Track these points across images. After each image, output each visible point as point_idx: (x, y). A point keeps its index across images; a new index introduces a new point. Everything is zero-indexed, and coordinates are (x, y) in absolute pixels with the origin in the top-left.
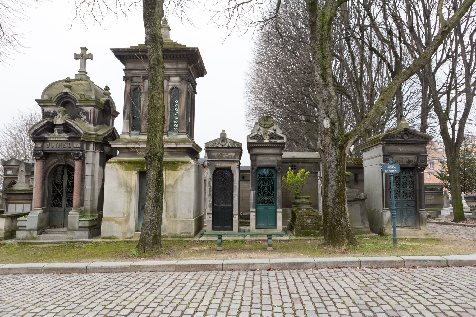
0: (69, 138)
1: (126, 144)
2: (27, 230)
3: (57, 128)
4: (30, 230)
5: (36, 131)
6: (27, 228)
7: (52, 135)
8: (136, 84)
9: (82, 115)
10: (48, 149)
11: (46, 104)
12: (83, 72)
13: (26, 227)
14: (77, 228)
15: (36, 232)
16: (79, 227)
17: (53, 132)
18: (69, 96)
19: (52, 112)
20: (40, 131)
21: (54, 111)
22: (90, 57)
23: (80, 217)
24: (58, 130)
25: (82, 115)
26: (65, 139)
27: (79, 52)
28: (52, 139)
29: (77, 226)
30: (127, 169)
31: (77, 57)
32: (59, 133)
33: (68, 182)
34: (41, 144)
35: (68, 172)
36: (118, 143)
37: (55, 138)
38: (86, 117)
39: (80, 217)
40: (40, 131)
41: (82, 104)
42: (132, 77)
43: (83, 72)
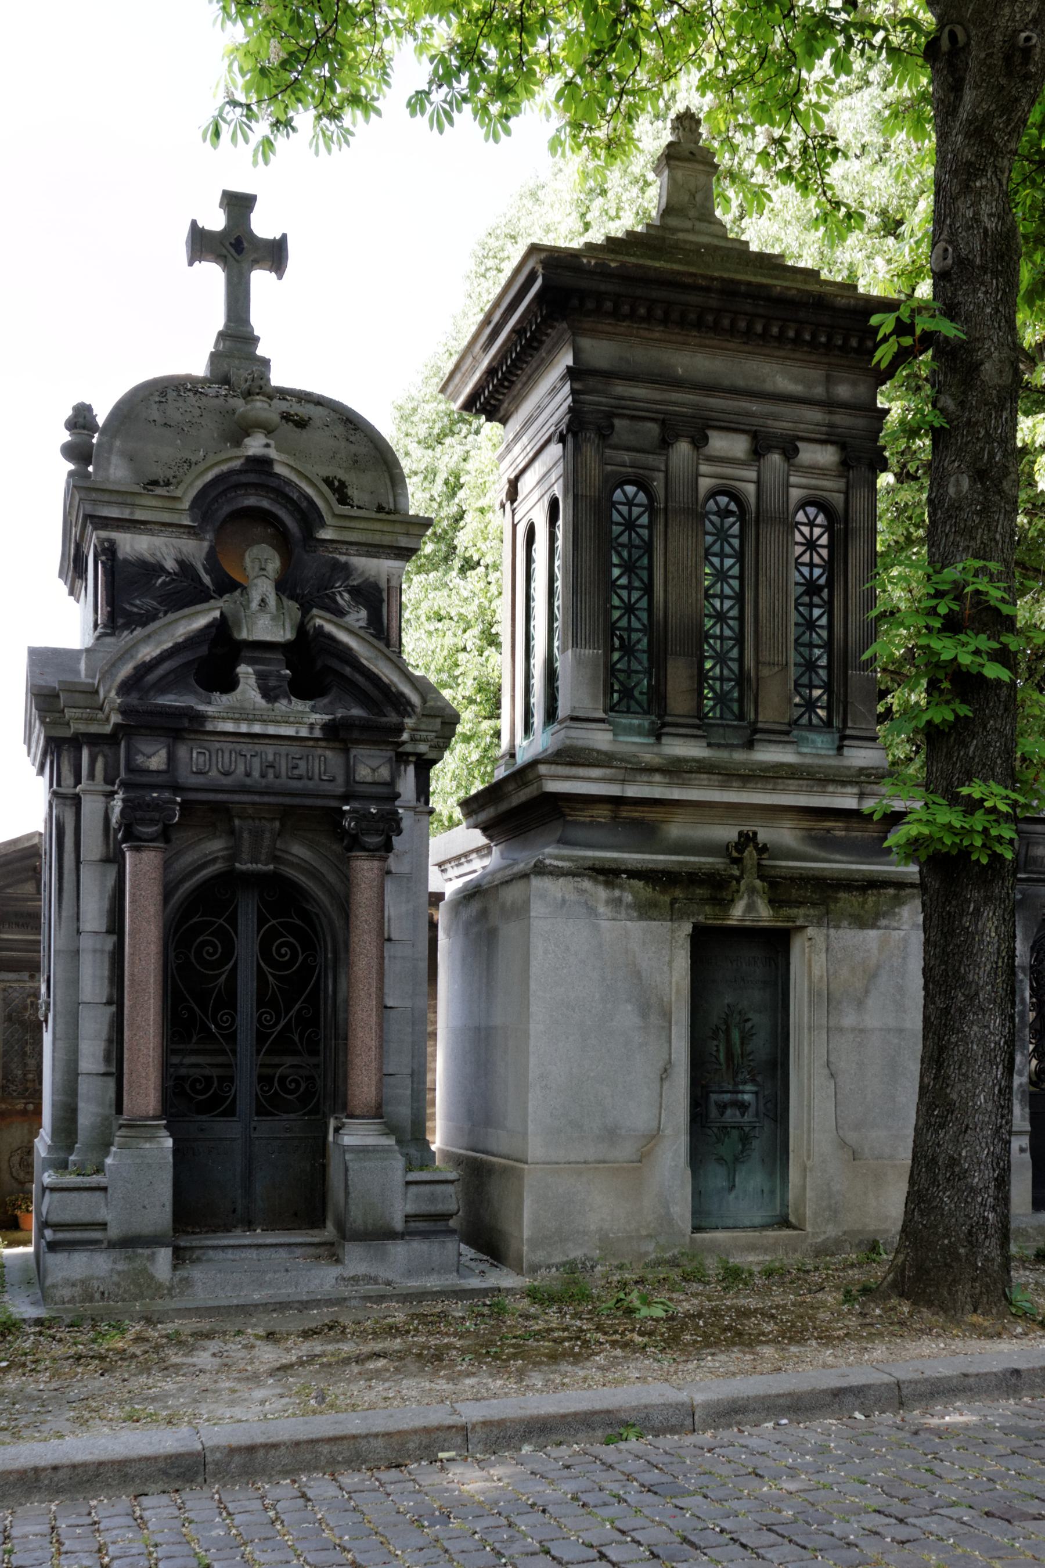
0: (325, 727)
1: (623, 781)
2: (112, 1245)
3: (251, 662)
4: (129, 1243)
5: (145, 669)
6: (114, 1232)
7: (223, 701)
8: (626, 457)
9: (344, 599)
10: (200, 780)
11: (139, 515)
12: (237, 338)
13: (103, 1226)
14: (399, 1225)
15: (164, 1255)
16: (408, 1218)
17: (230, 685)
18: (273, 483)
19: (170, 565)
20: (161, 671)
21: (181, 563)
22: (275, 255)
23: (409, 1169)
24: (261, 677)
25: (344, 599)
26: (304, 732)
27: (216, 221)
28: (229, 727)
29: (398, 1209)
30: (645, 910)
31: (202, 245)
32: (269, 694)
33: (261, 974)
34: (163, 753)
35: (262, 921)
36: (581, 771)
37: (251, 721)
38: (364, 613)
39: (409, 1169)
40: (161, 671)
41: (353, 537)
42: (610, 416)
43: (237, 338)
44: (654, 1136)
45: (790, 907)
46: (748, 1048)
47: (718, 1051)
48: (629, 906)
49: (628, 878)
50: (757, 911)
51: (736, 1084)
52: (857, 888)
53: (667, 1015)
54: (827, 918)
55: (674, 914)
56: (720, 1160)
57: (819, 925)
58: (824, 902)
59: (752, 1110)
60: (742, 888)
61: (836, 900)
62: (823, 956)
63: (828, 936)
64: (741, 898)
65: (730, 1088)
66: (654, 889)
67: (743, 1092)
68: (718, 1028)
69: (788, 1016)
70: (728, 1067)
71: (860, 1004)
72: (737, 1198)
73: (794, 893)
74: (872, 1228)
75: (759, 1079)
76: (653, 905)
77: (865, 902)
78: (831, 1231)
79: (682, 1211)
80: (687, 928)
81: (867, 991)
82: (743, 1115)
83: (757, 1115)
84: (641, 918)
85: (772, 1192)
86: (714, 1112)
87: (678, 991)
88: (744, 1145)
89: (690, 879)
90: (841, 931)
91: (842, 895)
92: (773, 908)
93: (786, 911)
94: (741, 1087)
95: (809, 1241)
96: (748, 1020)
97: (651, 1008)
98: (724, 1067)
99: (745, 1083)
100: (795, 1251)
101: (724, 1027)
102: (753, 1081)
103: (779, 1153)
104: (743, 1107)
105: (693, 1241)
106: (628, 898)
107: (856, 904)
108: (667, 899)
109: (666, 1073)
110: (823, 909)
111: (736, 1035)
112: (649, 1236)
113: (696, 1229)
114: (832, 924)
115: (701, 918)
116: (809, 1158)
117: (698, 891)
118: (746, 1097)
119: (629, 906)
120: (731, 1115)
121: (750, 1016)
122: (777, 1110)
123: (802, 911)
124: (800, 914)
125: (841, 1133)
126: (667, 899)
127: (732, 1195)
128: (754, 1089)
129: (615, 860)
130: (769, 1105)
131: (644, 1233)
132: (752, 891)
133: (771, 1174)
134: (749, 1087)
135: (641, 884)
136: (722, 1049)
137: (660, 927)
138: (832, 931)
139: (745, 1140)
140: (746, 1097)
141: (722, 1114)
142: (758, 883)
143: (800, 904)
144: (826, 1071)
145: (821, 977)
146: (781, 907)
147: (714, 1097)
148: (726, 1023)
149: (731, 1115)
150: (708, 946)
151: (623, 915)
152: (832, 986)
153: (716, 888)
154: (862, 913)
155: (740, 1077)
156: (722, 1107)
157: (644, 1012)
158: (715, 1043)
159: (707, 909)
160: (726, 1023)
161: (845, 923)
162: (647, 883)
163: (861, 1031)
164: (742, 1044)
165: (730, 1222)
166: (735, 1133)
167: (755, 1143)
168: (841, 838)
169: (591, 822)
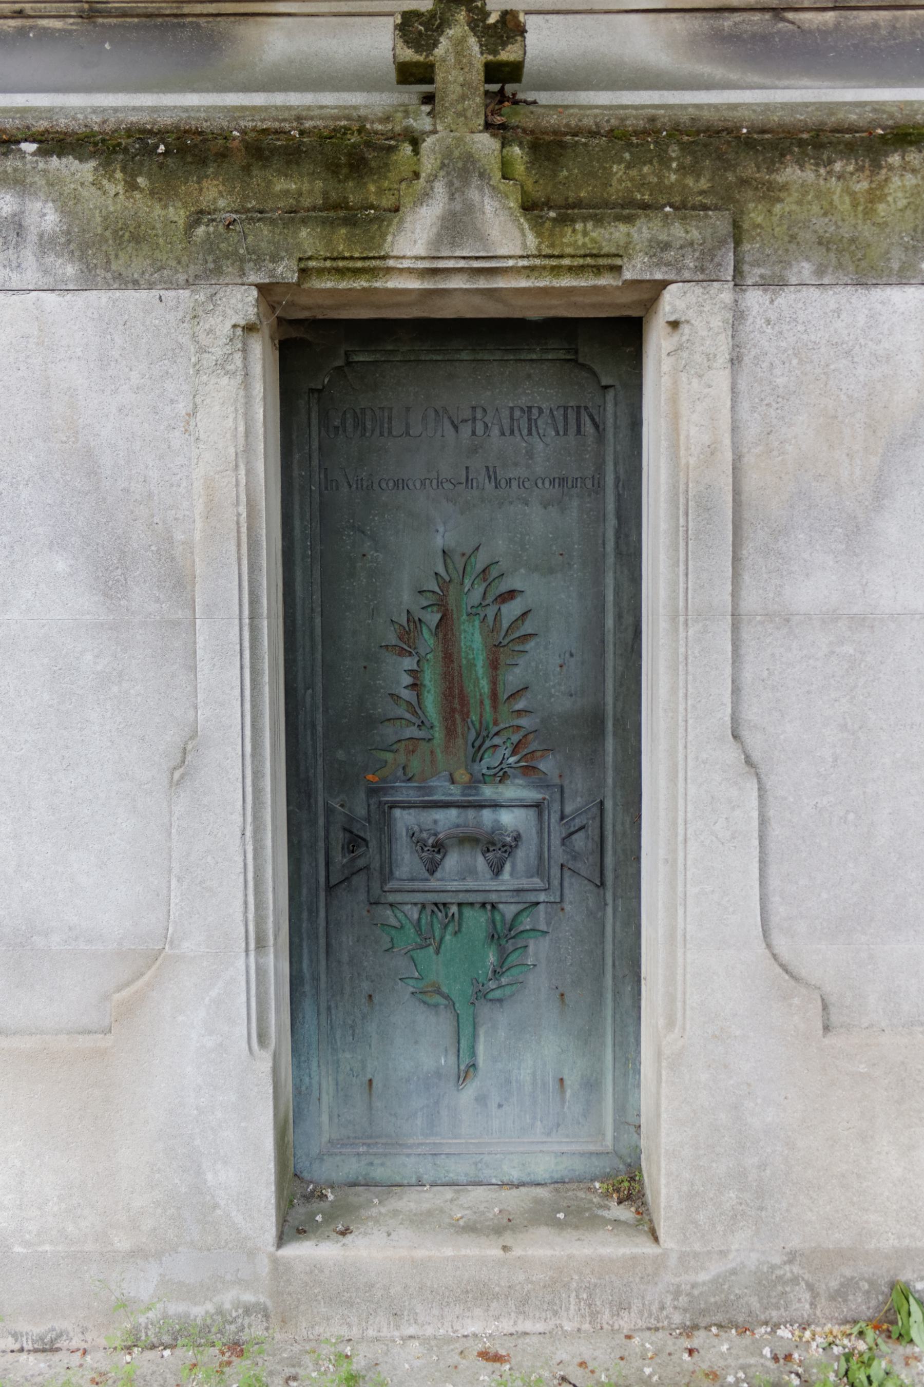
30: (105, 254)
44: (148, 960)
45: (599, 221)
46: (513, 678)
47: (415, 686)
48: (46, 244)
49: (44, 152)
50: (482, 238)
51: (476, 781)
52: (850, 150)
53: (179, 583)
54: (739, 257)
55: (213, 264)
56: (429, 994)
57: (705, 276)
58: (726, 199)
59: (525, 855)
60: (428, 163)
61: (771, 193)
62: (721, 379)
63: (738, 315)
64: (425, 196)
65: (455, 793)
66: (132, 186)
67: (495, 805)
68: (415, 623)
69: (636, 580)
70: (450, 732)
71: (854, 535)
72: (482, 1099)
73: (620, 177)
74: (889, 1242)
75: (547, 765)
76: (129, 235)
77: (875, 196)
78: (745, 1251)
79: (246, 1180)
80: (240, 302)
81: (880, 494)
82: (497, 870)
83: (540, 868)
84: (87, 282)
85: (592, 1085)
86: (407, 861)
87: (211, 510)
88: (503, 957)
89: (264, 149)
90: (786, 299)
91: (791, 174)
92: (537, 225)
93: (582, 236)
94: (488, 792)
95: (668, 1278)
96: (511, 594)
97: (126, 562)
98: (438, 734)
99: (503, 777)
100: (622, 1307)
101: (433, 618)
102: (529, 770)
103: (611, 974)
104: (497, 848)
105: (279, 1269)
106: (45, 216)
107: (844, 204)
108: (178, 214)
109: (183, 766)
110: (720, 222)
111: (472, 641)
112: (137, 1254)
113: (291, 1228)
114: (753, 274)
115: (286, 271)
116: (671, 1023)
117: (281, 185)
118: (508, 818)
119: (46, 244)
120: (461, 872)
121: (514, 582)
122: (603, 854)
123: (642, 231)
124: (636, 247)
125: (781, 943)
126: (178, 214)
127: (470, 1091)
128: (533, 795)
129: (23, 111)
130: (579, 841)
131: (122, 1243)
132: (461, 169)
133: (588, 1036)
134: (511, 791)
135: (86, 169)
136: (430, 678)
137: (150, 313)
138: (754, 299)
139: (505, 937)
140: (508, 818)
141: (433, 868)
142: (485, 144)
143: (630, 209)
144: (731, 754)
145: (712, 450)
146: (564, 220)
147: (404, 819)
148: (442, 605)
149: (461, 872)
150: (332, 368)
151: (31, 275)
152: (752, 481)
153: (346, 167)
154: (867, 231)
155: (490, 760)
156: (434, 851)
157: (109, 573)
158: (409, 663)
159: (308, 239)
160: (442, 605)
161: (805, 269)
162: (106, 164)
163: (860, 621)
164: (494, 665)
165: (459, 1169)
166: (476, 921)
167: (538, 950)
168: (824, 32)
169: (22, 32)
